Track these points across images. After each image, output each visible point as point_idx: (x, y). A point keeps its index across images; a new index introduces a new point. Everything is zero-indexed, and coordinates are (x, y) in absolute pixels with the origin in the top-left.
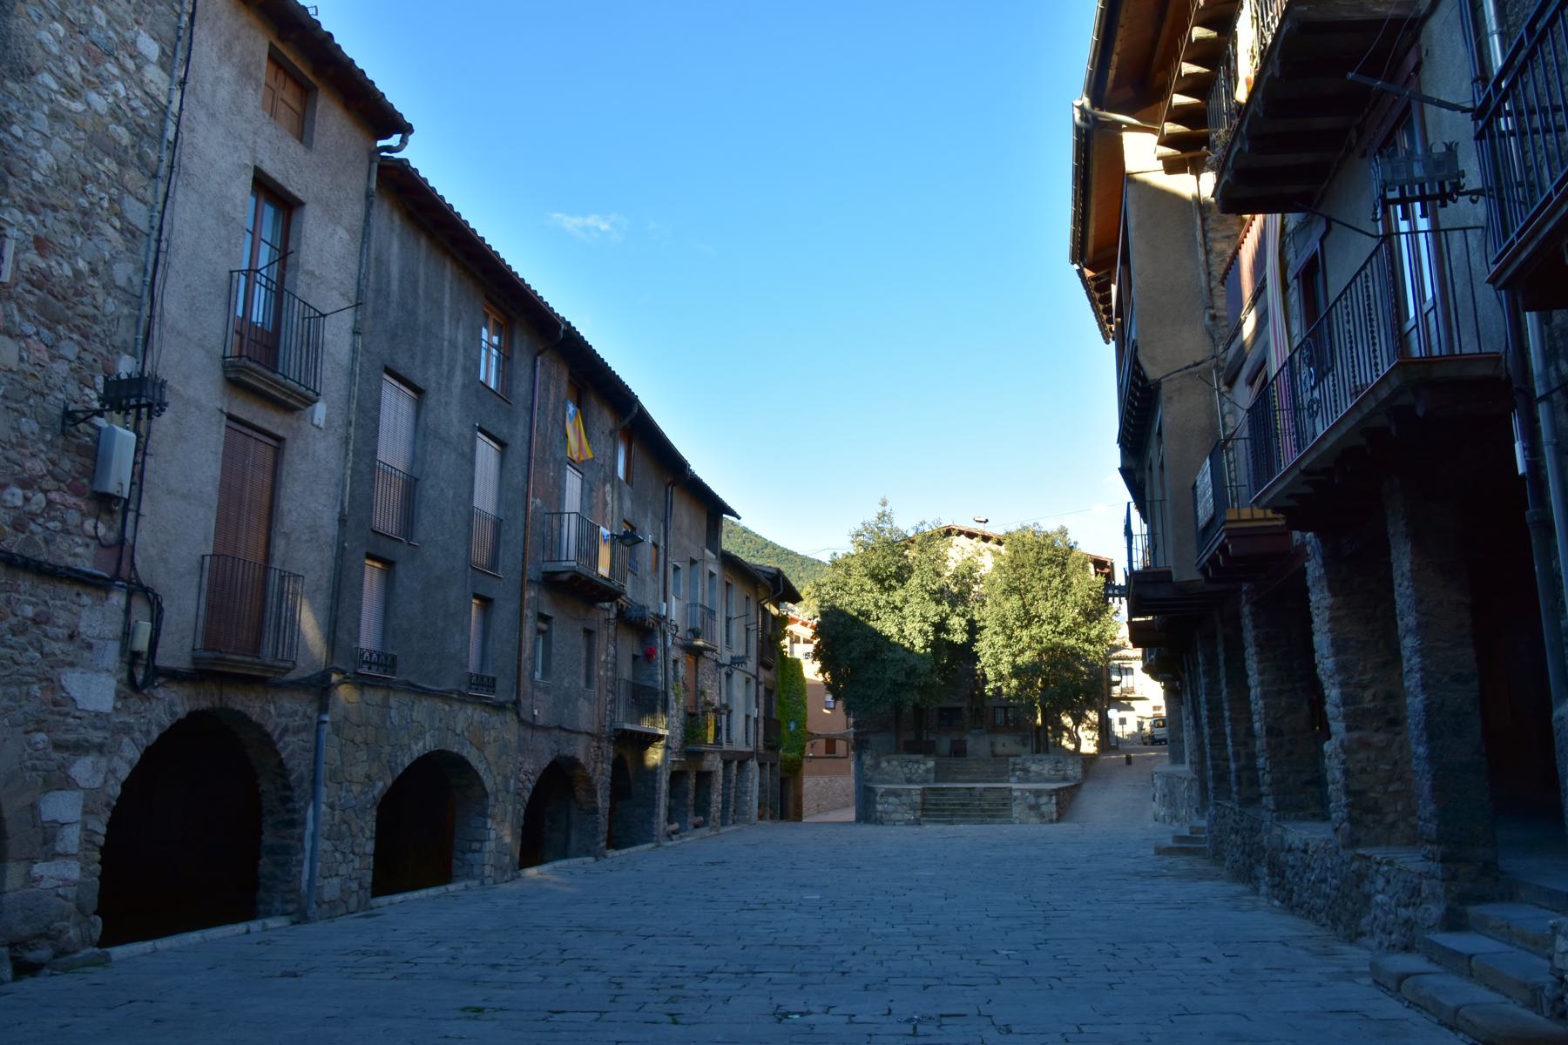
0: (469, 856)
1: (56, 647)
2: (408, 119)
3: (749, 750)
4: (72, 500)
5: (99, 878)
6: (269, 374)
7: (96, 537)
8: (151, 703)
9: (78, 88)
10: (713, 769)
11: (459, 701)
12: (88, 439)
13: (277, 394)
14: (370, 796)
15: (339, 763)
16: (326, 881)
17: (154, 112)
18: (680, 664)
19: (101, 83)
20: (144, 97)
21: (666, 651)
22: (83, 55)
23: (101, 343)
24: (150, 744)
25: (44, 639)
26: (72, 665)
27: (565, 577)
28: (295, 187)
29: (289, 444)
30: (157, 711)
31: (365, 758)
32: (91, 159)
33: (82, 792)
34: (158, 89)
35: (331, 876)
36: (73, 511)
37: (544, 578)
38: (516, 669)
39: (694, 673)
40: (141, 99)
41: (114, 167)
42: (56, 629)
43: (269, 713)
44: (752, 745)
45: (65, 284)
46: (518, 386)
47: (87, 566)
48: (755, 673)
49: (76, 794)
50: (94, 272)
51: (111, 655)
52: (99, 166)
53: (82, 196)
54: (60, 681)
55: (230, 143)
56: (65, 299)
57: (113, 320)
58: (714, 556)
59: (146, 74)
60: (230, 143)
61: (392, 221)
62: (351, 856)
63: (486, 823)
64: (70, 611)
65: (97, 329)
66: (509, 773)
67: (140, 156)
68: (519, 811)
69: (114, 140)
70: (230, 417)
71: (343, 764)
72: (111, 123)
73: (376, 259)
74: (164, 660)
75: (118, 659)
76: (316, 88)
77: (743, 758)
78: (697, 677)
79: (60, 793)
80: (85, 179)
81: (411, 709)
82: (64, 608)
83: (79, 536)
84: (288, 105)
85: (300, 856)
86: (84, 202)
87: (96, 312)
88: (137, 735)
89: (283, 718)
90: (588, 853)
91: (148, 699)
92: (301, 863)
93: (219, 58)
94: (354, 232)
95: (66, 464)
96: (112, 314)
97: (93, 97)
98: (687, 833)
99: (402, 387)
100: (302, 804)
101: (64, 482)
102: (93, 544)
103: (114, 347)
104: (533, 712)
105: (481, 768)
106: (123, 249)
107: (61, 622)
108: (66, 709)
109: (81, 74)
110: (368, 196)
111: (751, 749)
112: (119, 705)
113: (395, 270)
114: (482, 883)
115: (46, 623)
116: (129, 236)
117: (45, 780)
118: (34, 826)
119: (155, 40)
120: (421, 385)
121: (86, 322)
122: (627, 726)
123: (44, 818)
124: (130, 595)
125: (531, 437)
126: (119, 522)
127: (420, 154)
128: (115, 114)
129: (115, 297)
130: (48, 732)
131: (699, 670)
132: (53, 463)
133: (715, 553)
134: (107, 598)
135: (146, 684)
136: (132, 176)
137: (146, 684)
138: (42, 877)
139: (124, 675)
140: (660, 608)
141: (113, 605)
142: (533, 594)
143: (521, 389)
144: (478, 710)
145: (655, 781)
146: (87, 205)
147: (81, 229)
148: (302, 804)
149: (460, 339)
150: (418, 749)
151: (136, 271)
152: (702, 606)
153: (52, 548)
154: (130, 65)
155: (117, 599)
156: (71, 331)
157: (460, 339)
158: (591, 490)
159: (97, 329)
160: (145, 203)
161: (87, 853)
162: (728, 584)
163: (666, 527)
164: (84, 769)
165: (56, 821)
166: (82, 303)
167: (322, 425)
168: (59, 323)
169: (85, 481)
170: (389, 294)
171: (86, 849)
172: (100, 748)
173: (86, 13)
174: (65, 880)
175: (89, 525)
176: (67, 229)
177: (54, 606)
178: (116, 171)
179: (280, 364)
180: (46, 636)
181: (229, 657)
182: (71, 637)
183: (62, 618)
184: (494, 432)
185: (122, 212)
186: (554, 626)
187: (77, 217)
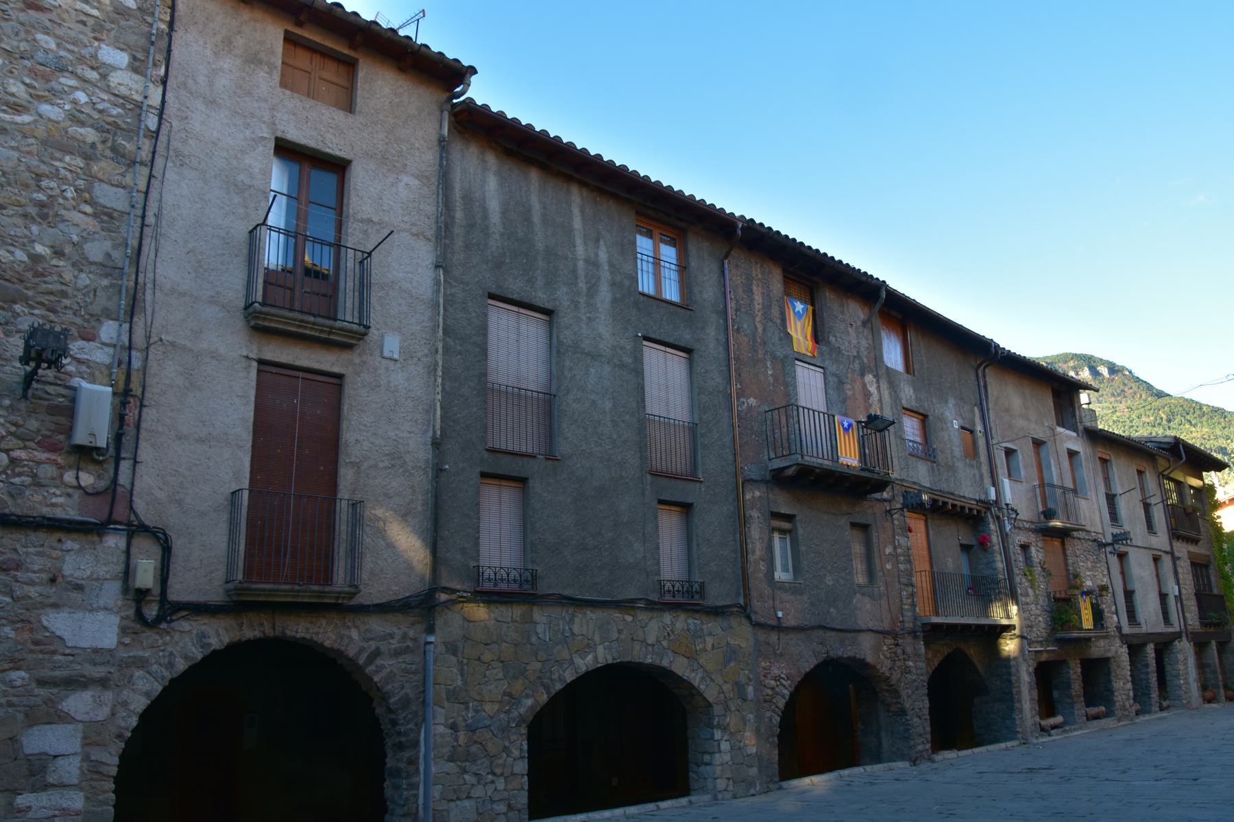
0: (702, 769)
1: (33, 591)
2: (466, 63)
3: (1171, 630)
4: (42, 455)
5: (114, 806)
6: (330, 323)
7: (80, 487)
8: (172, 637)
9: (25, 103)
10: (1109, 655)
11: (646, 609)
12: (61, 400)
13: (313, 333)
14: (516, 714)
15: (459, 683)
16: (452, 805)
17: (129, 110)
18: (1033, 550)
19: (54, 95)
20: (113, 98)
21: (1004, 537)
22: (28, 76)
23: (75, 314)
24: (175, 676)
25: (14, 584)
26: (55, 606)
27: (790, 472)
28: (334, 146)
29: (348, 381)
30: (181, 644)
31: (501, 675)
32: (47, 159)
33: (80, 725)
34: (130, 89)
35: (458, 799)
36: (46, 466)
37: (773, 476)
38: (740, 572)
39: (1061, 557)
40: (109, 101)
41: (80, 162)
42: (30, 574)
43: (350, 638)
44: (1176, 624)
45: (19, 269)
46: (701, 292)
47: (73, 514)
48: (1168, 549)
49: (70, 727)
50: (59, 253)
51: (111, 593)
52: (57, 164)
53: (38, 192)
54: (40, 621)
55: (239, 122)
56: (22, 281)
57: (88, 292)
58: (1074, 434)
59: (111, 79)
60: (239, 122)
61: (484, 161)
62: (490, 777)
63: (713, 734)
64: (50, 557)
65: (67, 302)
66: (743, 680)
67: (114, 149)
68: (770, 719)
69: (77, 140)
70: (261, 362)
71: (465, 683)
72: (71, 126)
73: (463, 198)
74: (179, 591)
75: (120, 597)
76: (357, 60)
77: (1164, 645)
78: (1066, 560)
79: (48, 726)
80: (39, 177)
81: (571, 621)
82: (38, 554)
83: (57, 487)
84: (337, 85)
85: (415, 780)
86: (41, 197)
87: (64, 288)
88: (155, 667)
89: (371, 642)
90: (903, 758)
91: (168, 633)
92: (415, 786)
93: (216, 54)
94: (427, 178)
95: (33, 424)
96: (86, 287)
97: (45, 108)
98: (1076, 726)
99: (522, 310)
100: (411, 726)
101: (32, 440)
102: (77, 495)
103: (92, 315)
104: (776, 614)
105: (695, 679)
106: (98, 229)
107: (36, 567)
108: (52, 648)
109: (27, 92)
110: (443, 144)
111: (1175, 628)
112: (127, 640)
113: (494, 205)
114: (715, 798)
115: (16, 570)
116: (106, 218)
117: (27, 715)
118: (16, 759)
119: (122, 50)
120: (549, 306)
121: (52, 298)
122: (935, 620)
123: (28, 751)
124: (130, 538)
125: (727, 340)
126: (112, 471)
127: (478, 92)
128: (75, 118)
129: (90, 272)
130: (28, 670)
131: (1068, 552)
132: (15, 424)
133: (1075, 430)
134: (101, 541)
135: (159, 619)
136: (103, 167)
137: (159, 619)
138: (30, 807)
139: (131, 612)
140: (986, 493)
141: (110, 547)
142: (757, 494)
143: (708, 292)
144: (244, 617)
145: (1010, 674)
146: (45, 198)
147: (39, 220)
148: (411, 726)
149: (603, 256)
150: (585, 663)
151: (115, 247)
152: (1062, 487)
153: (19, 501)
154: (93, 75)
155: (114, 541)
156: (32, 307)
157: (603, 256)
158: (841, 382)
159: (67, 302)
160: (124, 187)
161: (93, 783)
162: (1104, 461)
163: (982, 411)
164: (79, 703)
165: (46, 754)
166: (45, 282)
167: (396, 356)
168: (15, 302)
169: (61, 437)
170: (487, 227)
171: (92, 779)
172: (103, 683)
173: (28, 41)
174: (64, 809)
175: (69, 477)
176: (19, 221)
177: (27, 553)
178: (82, 165)
179: (340, 310)
180: (17, 581)
181: (254, 586)
182: (53, 580)
183: (38, 563)
184: (671, 340)
185: (92, 198)
186: (798, 525)
187: (33, 211)
